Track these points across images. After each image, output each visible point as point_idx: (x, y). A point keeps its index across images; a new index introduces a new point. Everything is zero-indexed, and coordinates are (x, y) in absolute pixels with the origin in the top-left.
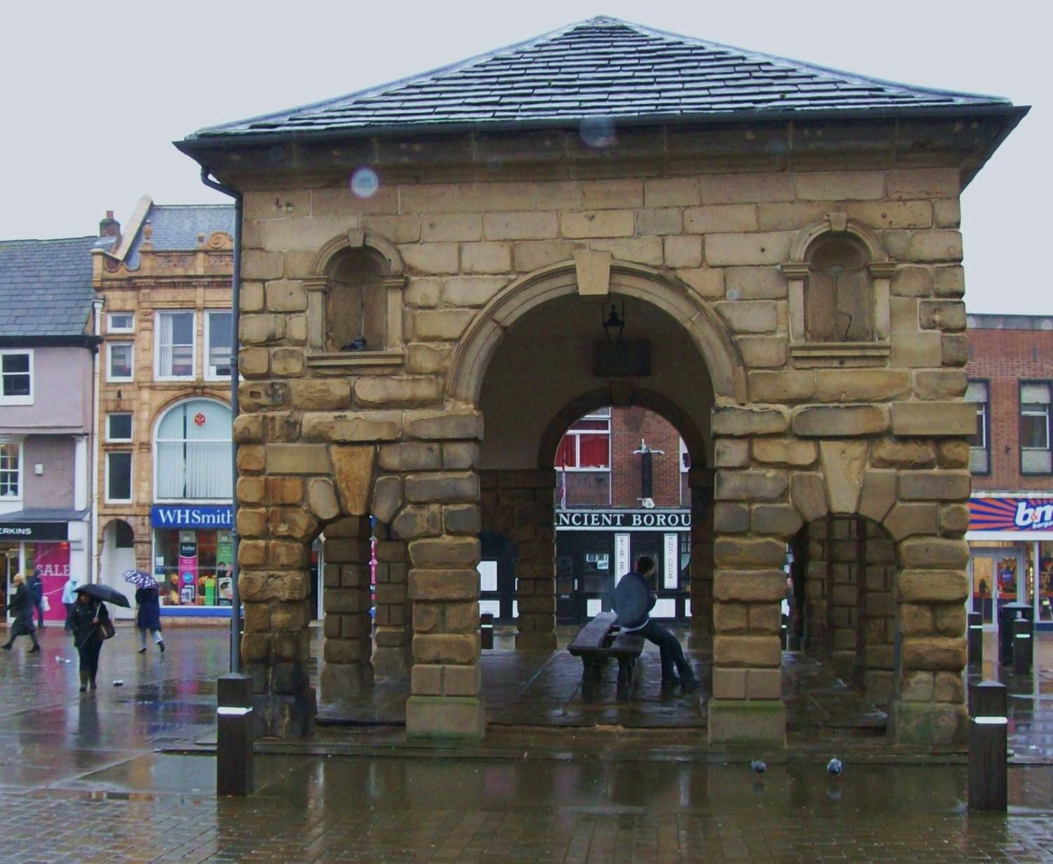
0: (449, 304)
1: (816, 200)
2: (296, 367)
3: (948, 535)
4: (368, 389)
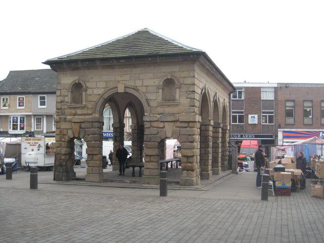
0: (94, 94)
1: (166, 71)
2: (66, 107)
3: (190, 142)
4: (79, 111)
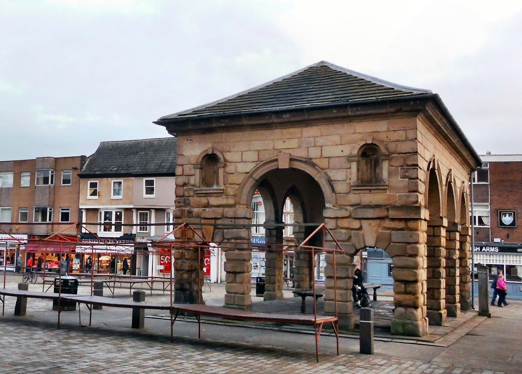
0: (238, 173)
3: (411, 256)
4: (213, 201)
